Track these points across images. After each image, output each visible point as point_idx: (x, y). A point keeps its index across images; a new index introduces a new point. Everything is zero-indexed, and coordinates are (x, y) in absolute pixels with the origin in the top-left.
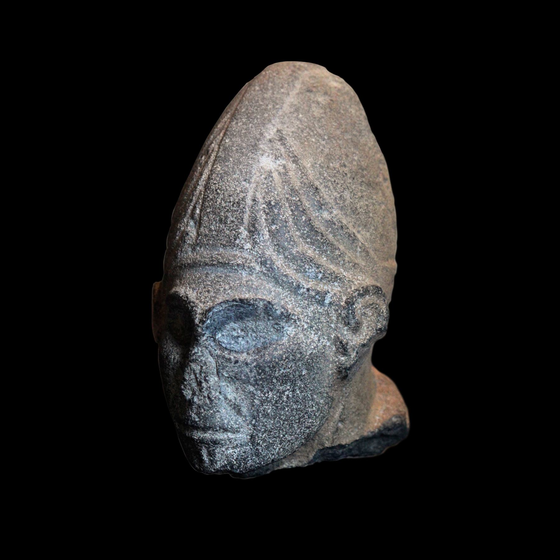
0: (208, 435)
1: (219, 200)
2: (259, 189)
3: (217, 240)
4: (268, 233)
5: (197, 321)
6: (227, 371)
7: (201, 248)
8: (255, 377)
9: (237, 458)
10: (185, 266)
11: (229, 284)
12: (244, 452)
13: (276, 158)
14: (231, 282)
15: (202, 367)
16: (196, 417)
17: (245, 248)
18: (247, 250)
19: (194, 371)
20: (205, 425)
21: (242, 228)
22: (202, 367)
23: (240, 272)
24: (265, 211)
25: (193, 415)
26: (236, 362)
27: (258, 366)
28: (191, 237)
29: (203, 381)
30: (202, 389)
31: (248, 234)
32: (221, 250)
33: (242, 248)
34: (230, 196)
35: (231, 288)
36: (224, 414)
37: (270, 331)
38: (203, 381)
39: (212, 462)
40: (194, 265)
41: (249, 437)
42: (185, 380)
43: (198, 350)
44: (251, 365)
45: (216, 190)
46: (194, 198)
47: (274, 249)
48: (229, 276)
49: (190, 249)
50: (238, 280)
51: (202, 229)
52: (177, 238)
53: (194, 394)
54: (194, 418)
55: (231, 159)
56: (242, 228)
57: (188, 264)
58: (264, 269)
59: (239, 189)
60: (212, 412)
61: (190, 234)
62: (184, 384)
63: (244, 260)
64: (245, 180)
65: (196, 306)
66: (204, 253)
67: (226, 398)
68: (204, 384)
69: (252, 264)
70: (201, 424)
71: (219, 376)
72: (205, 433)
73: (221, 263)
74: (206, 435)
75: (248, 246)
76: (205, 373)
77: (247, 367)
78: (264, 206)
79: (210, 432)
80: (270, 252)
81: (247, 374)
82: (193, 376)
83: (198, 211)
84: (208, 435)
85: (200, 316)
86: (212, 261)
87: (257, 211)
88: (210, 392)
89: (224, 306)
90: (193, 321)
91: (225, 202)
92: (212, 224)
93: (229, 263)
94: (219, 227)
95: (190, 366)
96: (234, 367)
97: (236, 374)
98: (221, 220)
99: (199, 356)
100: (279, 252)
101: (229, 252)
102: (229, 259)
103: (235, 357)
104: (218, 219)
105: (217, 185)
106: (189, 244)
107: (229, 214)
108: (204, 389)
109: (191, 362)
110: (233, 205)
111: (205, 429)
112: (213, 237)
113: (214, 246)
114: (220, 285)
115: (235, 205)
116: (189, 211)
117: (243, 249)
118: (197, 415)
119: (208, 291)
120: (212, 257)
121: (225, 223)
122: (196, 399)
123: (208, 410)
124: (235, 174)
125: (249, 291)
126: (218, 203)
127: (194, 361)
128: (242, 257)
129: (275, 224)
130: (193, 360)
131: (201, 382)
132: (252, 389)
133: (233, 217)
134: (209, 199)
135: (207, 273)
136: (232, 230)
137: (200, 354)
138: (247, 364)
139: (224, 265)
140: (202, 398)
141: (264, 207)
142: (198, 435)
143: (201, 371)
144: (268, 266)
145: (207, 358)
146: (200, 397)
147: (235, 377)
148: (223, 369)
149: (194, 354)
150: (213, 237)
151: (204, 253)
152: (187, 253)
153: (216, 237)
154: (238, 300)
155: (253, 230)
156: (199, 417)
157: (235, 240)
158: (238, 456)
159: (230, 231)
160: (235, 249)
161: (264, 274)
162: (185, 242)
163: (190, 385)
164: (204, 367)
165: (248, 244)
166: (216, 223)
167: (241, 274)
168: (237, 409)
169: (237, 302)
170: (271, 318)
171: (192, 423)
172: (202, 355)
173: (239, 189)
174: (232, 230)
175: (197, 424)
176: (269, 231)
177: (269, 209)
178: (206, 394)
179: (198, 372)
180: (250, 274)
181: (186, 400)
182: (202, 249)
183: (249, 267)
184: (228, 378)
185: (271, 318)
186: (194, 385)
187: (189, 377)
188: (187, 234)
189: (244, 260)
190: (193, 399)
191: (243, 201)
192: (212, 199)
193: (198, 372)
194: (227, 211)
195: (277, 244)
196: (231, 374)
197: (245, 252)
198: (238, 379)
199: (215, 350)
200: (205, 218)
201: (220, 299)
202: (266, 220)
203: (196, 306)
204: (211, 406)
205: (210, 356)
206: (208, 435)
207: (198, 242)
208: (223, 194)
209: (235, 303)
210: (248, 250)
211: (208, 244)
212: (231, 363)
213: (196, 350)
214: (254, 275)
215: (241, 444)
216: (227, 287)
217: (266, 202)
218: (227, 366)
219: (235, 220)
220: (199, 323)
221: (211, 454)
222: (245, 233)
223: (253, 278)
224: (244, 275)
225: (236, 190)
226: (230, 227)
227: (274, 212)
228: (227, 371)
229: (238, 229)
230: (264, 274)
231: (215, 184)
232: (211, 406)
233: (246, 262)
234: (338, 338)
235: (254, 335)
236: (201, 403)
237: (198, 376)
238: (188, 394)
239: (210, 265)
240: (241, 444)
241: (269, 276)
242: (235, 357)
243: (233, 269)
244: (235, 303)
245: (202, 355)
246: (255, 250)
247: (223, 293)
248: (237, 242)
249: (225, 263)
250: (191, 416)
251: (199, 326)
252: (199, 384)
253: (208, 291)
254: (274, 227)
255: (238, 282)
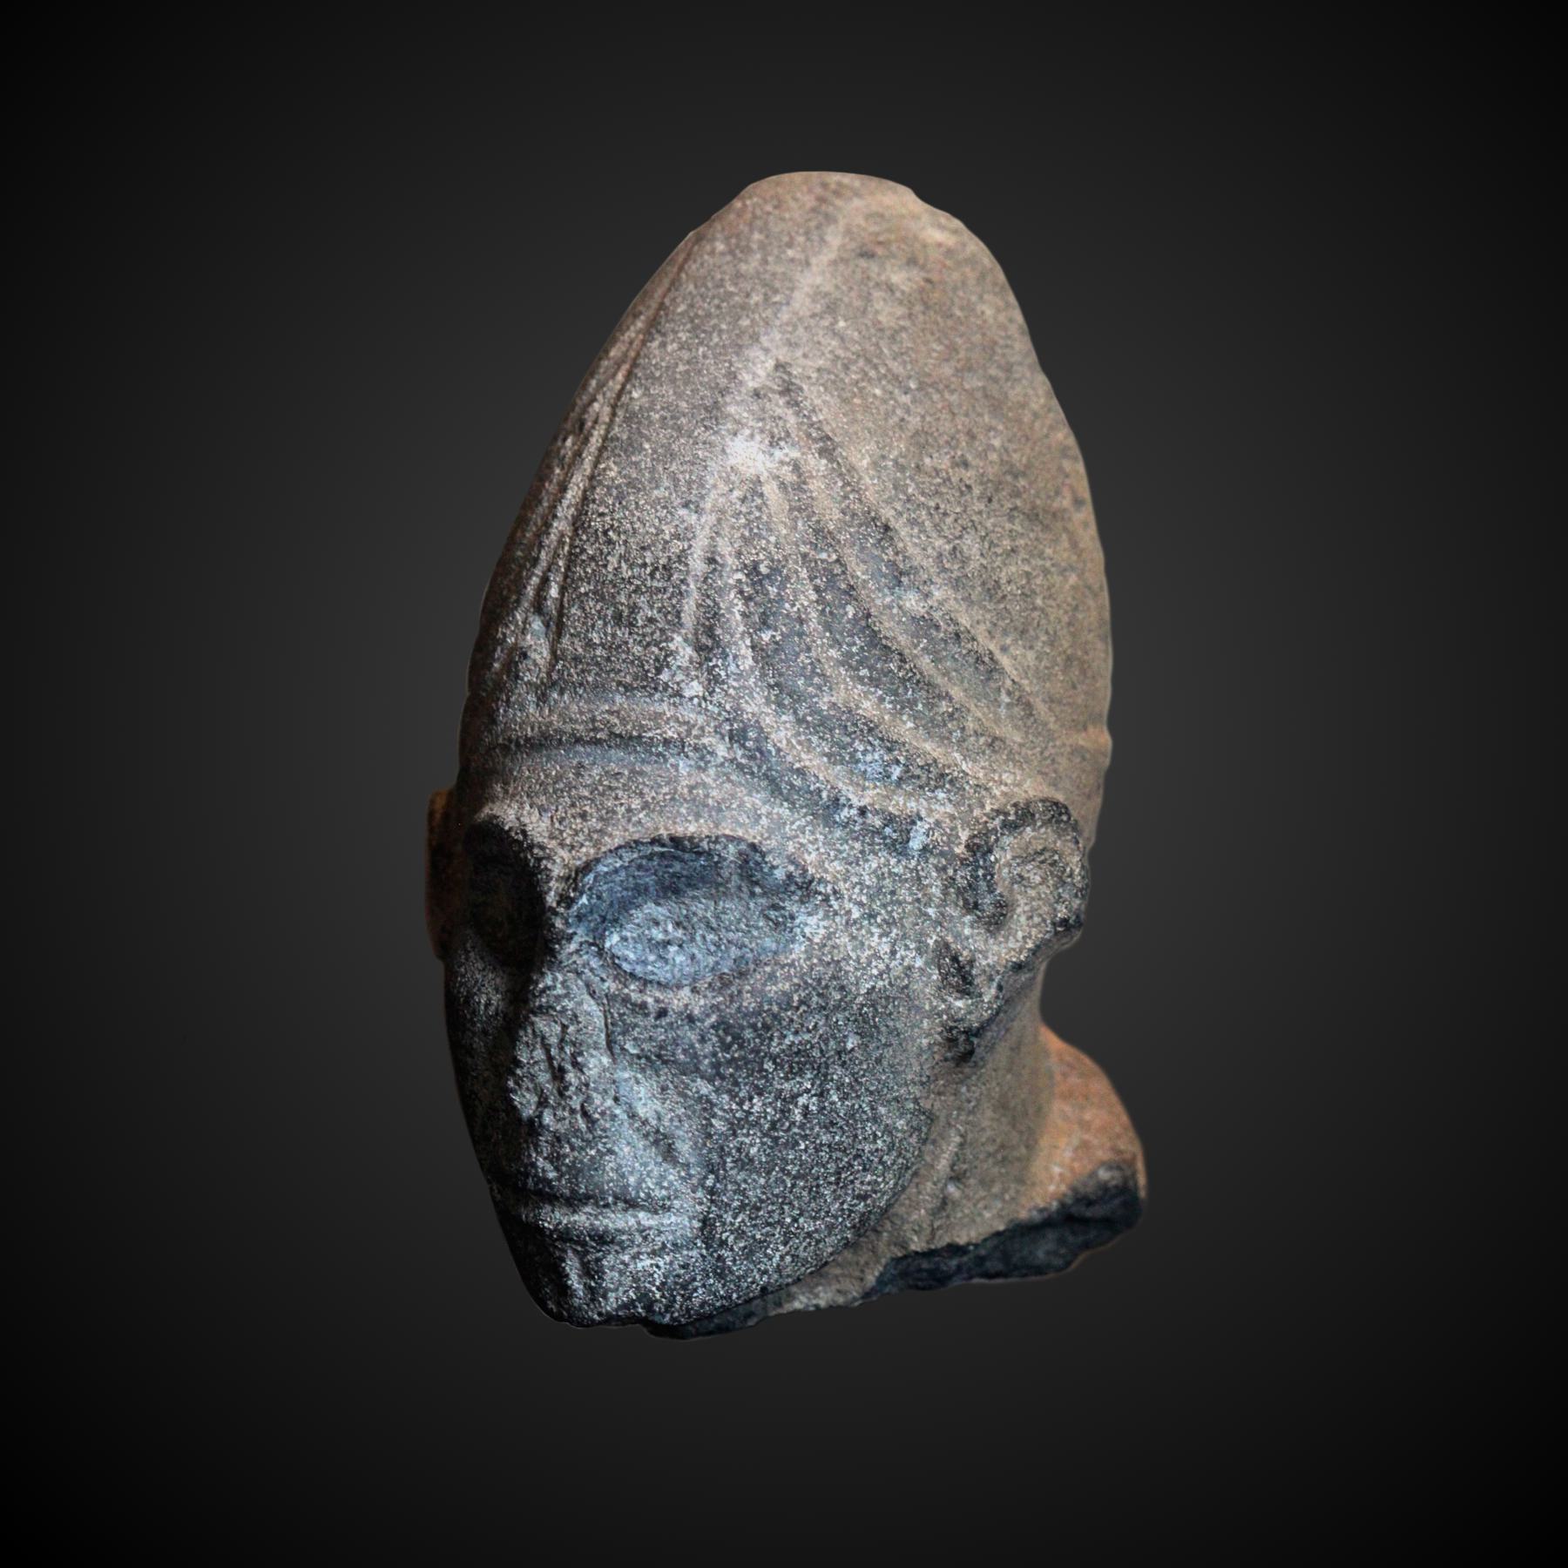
0: (582, 1219)
1: (613, 561)
2: (726, 531)
3: (608, 673)
4: (749, 653)
5: (551, 899)
6: (635, 1039)
7: (561, 693)
8: (714, 1054)
9: (663, 1284)
10: (518, 745)
11: (641, 794)
12: (683, 1267)
13: (774, 442)
14: (646, 790)
15: (565, 1027)
16: (548, 1167)
17: (687, 694)
18: (691, 699)
19: (543, 1038)
20: (573, 1191)
21: (678, 639)
22: (565, 1027)
23: (672, 760)
24: (741, 592)
25: (541, 1162)
26: (662, 1013)
27: (722, 1025)
28: (536, 664)
29: (568, 1067)
30: (566, 1088)
31: (695, 655)
32: (619, 699)
33: (678, 694)
34: (643, 548)
35: (646, 806)
36: (629, 1159)
37: (757, 928)
38: (568, 1067)
39: (594, 1293)
40: (543, 742)
41: (697, 1224)
42: (518, 1064)
43: (555, 979)
44: (702, 1021)
45: (605, 533)
46: (543, 554)
47: (767, 698)
48: (641, 773)
49: (531, 698)
50: (668, 783)
51: (565, 641)
52: (496, 665)
53: (543, 1103)
54: (544, 1171)
55: (647, 446)
56: (678, 639)
57: (527, 740)
58: (740, 753)
59: (668, 530)
60: (593, 1152)
61: (533, 655)
62: (514, 1074)
63: (683, 729)
64: (686, 505)
65: (549, 858)
66: (571, 710)
67: (633, 1116)
68: (571, 1077)
69: (705, 741)
70: (563, 1187)
71: (612, 1054)
72: (575, 1212)
73: (620, 736)
74: (576, 1217)
75: (695, 688)
76: (574, 1044)
77: (692, 1029)
78: (739, 576)
79: (588, 1209)
80: (756, 706)
81: (692, 1046)
82: (539, 1054)
83: (554, 592)
84: (582, 1219)
85: (561, 886)
86: (595, 729)
87: (720, 591)
88: (588, 1099)
89: (628, 856)
90: (540, 898)
91: (631, 567)
92: (593, 626)
93: (640, 737)
94: (614, 635)
95: (533, 1024)
96: (656, 1027)
97: (661, 1048)
98: (618, 617)
99: (558, 998)
100: (780, 704)
101: (642, 707)
102: (642, 726)
103: (657, 1001)
104: (609, 612)
105: (608, 518)
106: (529, 683)
107: (642, 600)
108: (572, 1089)
109: (535, 1014)
110: (652, 575)
111: (574, 1202)
112: (597, 664)
113: (599, 689)
114: (616, 798)
115: (658, 575)
116: (530, 591)
117: (682, 696)
118: (552, 1163)
119: (584, 816)
120: (593, 720)
121: (631, 625)
122: (548, 1119)
123: (582, 1148)
124: (657, 487)
125: (698, 816)
126: (610, 568)
127: (544, 1010)
128: (677, 720)
129: (769, 627)
130: (541, 1007)
131: (562, 1070)
132: (705, 1088)
133: (652, 607)
134: (584, 557)
135: (581, 765)
136: (649, 644)
137: (560, 991)
138: (691, 1019)
139: (626, 741)
140: (566, 1114)
141: (739, 581)
142: (554, 1218)
143: (562, 1040)
144: (749, 744)
145: (580, 1004)
146: (559, 1113)
147: (659, 1056)
148: (624, 1033)
149: (543, 991)
150: (597, 664)
151: (571, 710)
152: (522, 708)
153: (603, 663)
154: (667, 841)
155: (709, 644)
156: (557, 1169)
157: (659, 671)
158: (665, 1277)
159: (645, 648)
160: (657, 696)
161: (740, 767)
162: (517, 677)
163: (533, 1077)
164: (571, 1029)
165: (695, 683)
166: (605, 624)
167: (676, 767)
168: (665, 1146)
169: (663, 845)
170: (758, 890)
171: (536, 1184)
172: (567, 995)
173: (668, 530)
174: (649, 644)
175: (552, 1187)
176: (753, 647)
177: (753, 584)
178: (576, 1103)
179: (554, 1040)
180: (699, 768)
181: (520, 1120)
182: (566, 697)
183: (696, 749)
184: (639, 1057)
185: (758, 890)
186: (544, 1078)
187: (529, 1056)
188: (525, 656)
189: (683, 729)
190: (540, 1116)
191: (680, 562)
192: (592, 558)
193: (554, 1040)
194: (635, 591)
195: (777, 685)
196: (646, 1046)
197: (686, 706)
198: (665, 1062)
199: (603, 980)
200: (573, 611)
201: (617, 837)
202: (744, 615)
203: (549, 858)
204: (590, 1136)
205: (587, 997)
206: (584, 1218)
207: (555, 676)
208: (625, 542)
209: (657, 849)
210: (696, 701)
211: (581, 685)
212: (647, 1015)
213: (548, 981)
214: (712, 771)
215: (674, 1245)
216: (636, 803)
217: (746, 566)
218: (636, 1025)
219: (657, 616)
220: (559, 903)
221: (591, 1271)
222: (685, 654)
223: (709, 777)
224: (683, 771)
225: (660, 531)
226: (644, 635)
227: (767, 594)
228: (635, 1039)
229: (666, 641)
230: (740, 767)
231: (602, 515)
232: (590, 1136)
233: (689, 733)
234: (947, 946)
235: (711, 937)
236: (562, 1128)
237: (553, 1052)
238: (525, 1102)
239: (589, 743)
240: (674, 1245)
241: (752, 773)
242: (657, 1001)
243: (651, 753)
244: (657, 849)
245: (567, 995)
246: (714, 699)
247: (623, 822)
248: (665, 676)
249: (631, 738)
250: (534, 1165)
251: (556, 914)
252: (558, 1074)
253: (584, 816)
254: (766, 636)
255: (665, 790)
